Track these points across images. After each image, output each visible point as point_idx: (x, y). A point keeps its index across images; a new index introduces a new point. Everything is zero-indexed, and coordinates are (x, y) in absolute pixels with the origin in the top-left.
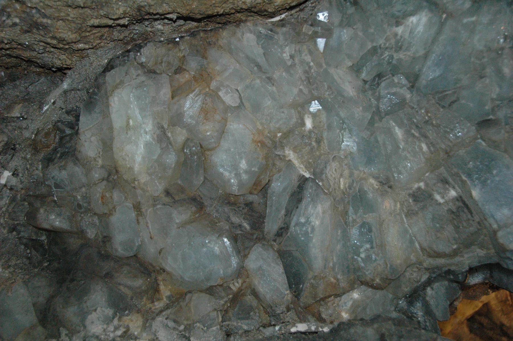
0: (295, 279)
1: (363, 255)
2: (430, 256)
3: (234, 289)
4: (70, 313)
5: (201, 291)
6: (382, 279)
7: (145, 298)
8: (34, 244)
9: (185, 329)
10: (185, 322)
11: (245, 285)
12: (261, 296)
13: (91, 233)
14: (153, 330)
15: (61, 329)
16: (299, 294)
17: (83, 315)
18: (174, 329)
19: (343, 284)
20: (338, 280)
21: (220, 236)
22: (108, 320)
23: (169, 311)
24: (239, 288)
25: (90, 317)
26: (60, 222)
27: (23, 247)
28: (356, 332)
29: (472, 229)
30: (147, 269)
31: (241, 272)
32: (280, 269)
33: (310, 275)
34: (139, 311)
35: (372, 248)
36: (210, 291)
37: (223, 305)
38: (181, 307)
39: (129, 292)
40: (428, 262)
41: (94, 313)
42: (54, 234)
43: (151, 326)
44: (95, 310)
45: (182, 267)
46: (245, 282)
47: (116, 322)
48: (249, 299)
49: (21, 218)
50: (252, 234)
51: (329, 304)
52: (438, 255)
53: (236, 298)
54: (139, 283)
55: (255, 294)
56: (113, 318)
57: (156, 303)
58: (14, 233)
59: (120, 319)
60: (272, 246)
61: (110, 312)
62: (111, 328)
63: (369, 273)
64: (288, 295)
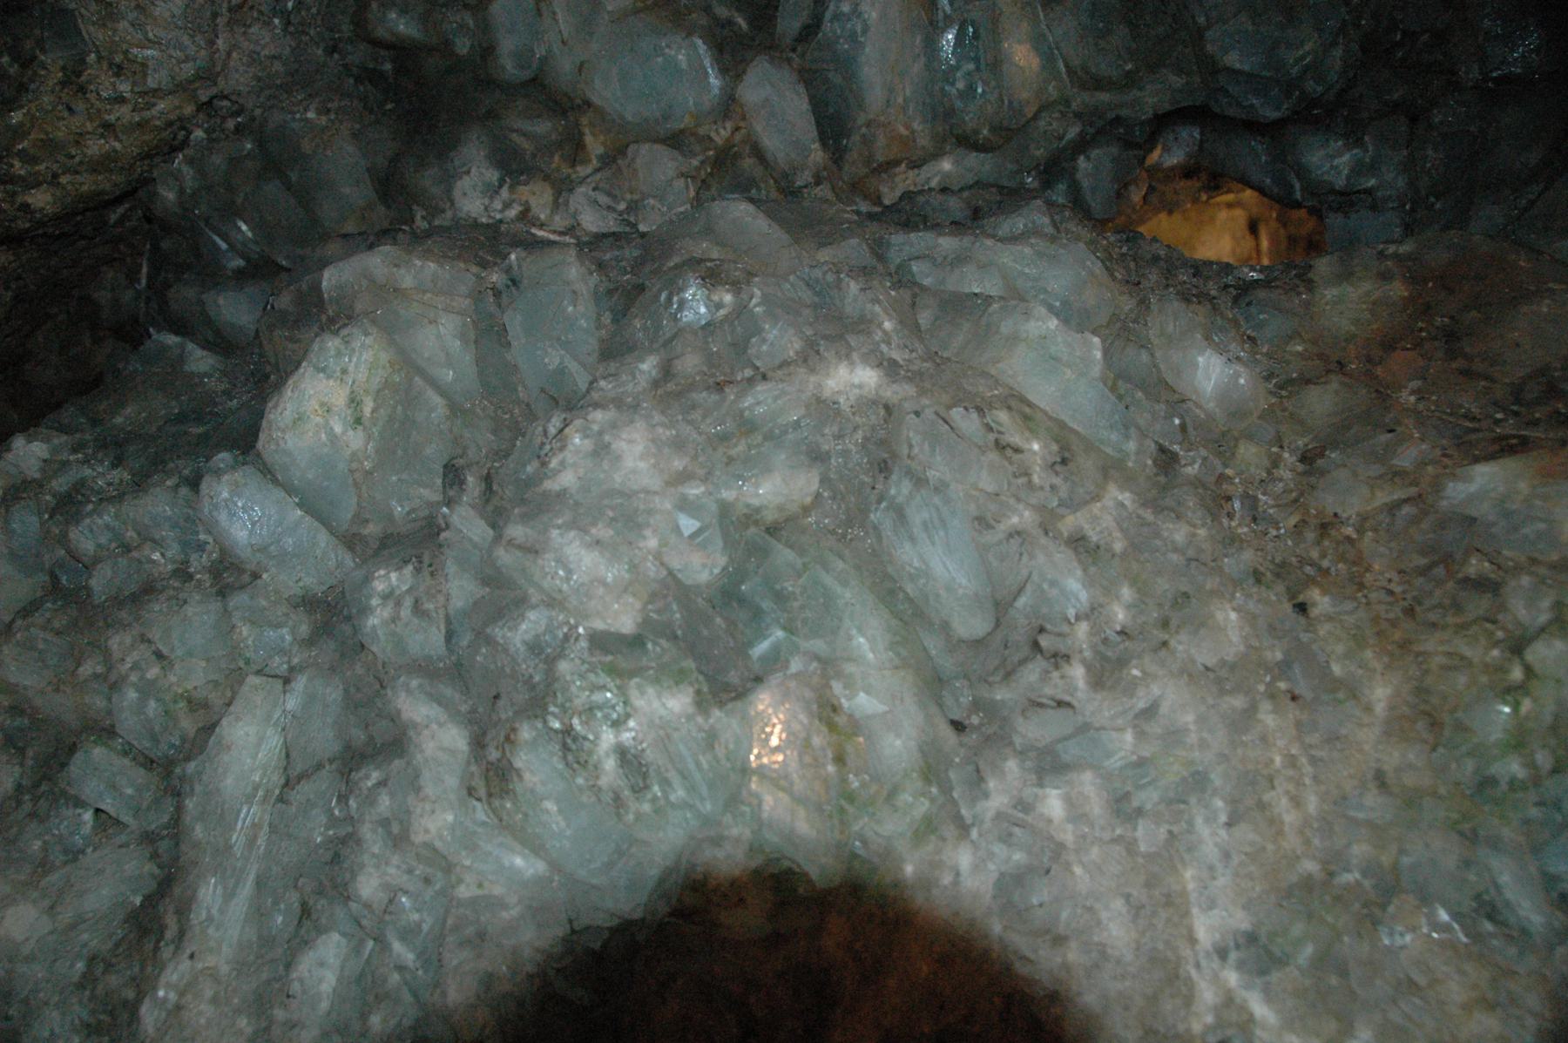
0: (832, 125)
1: (960, 85)
2: (1083, 87)
3: (719, 141)
4: (427, 181)
5: (656, 141)
6: (993, 129)
7: (556, 158)
8: (371, 76)
9: (629, 209)
10: (628, 196)
11: (738, 137)
12: (769, 157)
13: (463, 46)
14: (572, 209)
15: (415, 207)
16: (841, 158)
17: (448, 179)
18: (609, 208)
19: (924, 141)
20: (913, 132)
21: (689, 35)
22: (492, 191)
23: (598, 176)
24: (727, 140)
25: (459, 183)
26: (406, 24)
27: (351, 81)
28: (927, 202)
29: (1161, 29)
30: (564, 105)
31: (729, 106)
32: (803, 104)
33: (861, 120)
34: (546, 178)
35: (978, 69)
36: (675, 141)
37: (698, 169)
38: (619, 169)
39: (526, 145)
40: (1080, 100)
41: (466, 178)
42: (401, 50)
43: (567, 203)
44: (468, 172)
45: (619, 94)
46: (737, 129)
47: (505, 193)
48: (748, 163)
49: (345, 27)
50: (753, 40)
51: (897, 179)
52: (1098, 83)
53: (724, 160)
54: (543, 127)
55: (758, 153)
56: (500, 187)
57: (579, 168)
58: (336, 56)
59: (512, 188)
60: (789, 60)
61: (493, 175)
62: (498, 205)
63: (970, 119)
64: (818, 155)
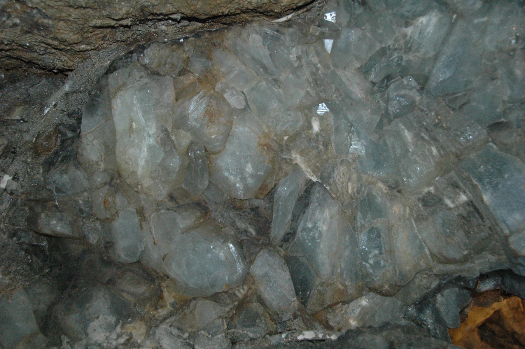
0: (302, 285)
1: (371, 261)
2: (440, 262)
3: (240, 296)
4: (72, 320)
5: (206, 298)
6: (391, 286)
7: (148, 305)
8: (35, 250)
9: (190, 337)
10: (190, 330)
11: (250, 291)
12: (267, 303)
13: (93, 239)
14: (157, 337)
15: (63, 336)
16: (306, 301)
17: (85, 322)
18: (178, 336)
19: (351, 291)
20: (346, 286)
21: (225, 241)
22: (111, 328)
23: (173, 319)
24: (245, 295)
25: (92, 324)
26: (61, 227)
27: (23, 253)
28: (364, 340)
30: (151, 276)
31: (247, 278)
32: (287, 275)
33: (318, 282)
34: (142, 319)
35: (381, 253)
36: (215, 298)
37: (229, 312)
38: (185, 314)
39: (132, 299)
40: (438, 268)
41: (96, 320)
42: (55, 239)
43: (154, 333)
44: (98, 318)
45: (186, 273)
46: (250, 288)
47: (118, 329)
48: (255, 306)
49: (22, 223)
50: (258, 240)
51: (337, 311)
52: (449, 261)
53: (242, 305)
54: (142, 289)
55: (261, 301)
56: (116, 326)
57: (160, 311)
58: (15, 238)
59: (123, 327)
60: (278, 252)
61: (112, 319)
62: (114, 336)
63: (377, 280)
64: (295, 302)
